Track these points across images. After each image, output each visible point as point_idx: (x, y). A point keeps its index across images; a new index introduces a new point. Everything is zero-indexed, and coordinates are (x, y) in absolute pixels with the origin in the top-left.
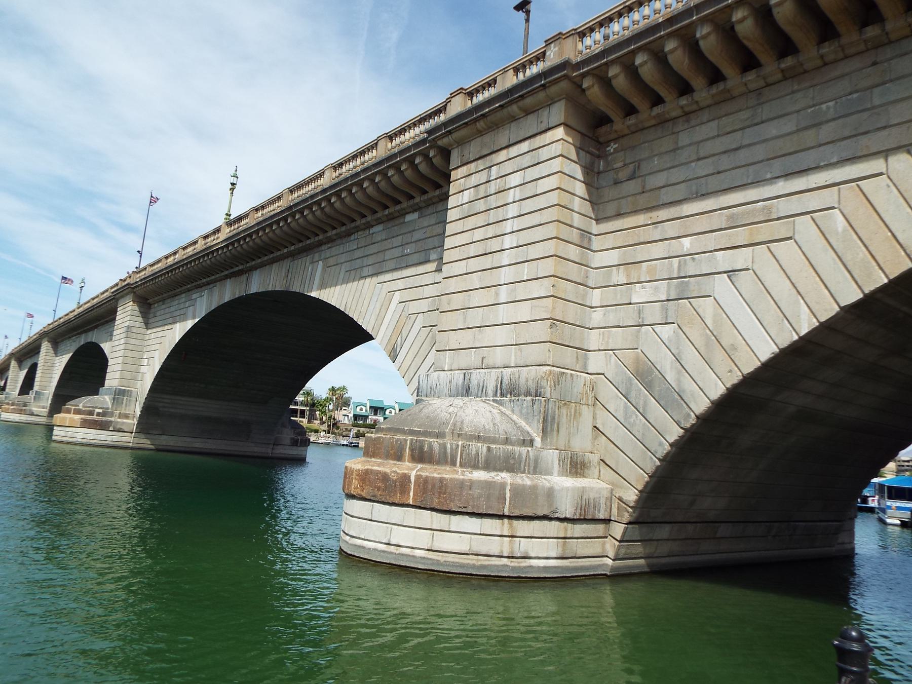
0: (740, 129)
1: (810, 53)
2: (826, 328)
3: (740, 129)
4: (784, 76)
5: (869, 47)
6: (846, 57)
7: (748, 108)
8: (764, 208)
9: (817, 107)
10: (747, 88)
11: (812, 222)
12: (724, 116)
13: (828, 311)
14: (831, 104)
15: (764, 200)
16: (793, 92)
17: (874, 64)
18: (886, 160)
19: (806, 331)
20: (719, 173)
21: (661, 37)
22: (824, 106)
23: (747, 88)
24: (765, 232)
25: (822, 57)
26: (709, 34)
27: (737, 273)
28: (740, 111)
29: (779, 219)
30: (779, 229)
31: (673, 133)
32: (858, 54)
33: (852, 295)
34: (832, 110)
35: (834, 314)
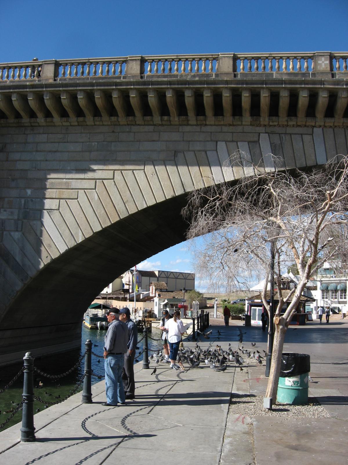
0: (57, 142)
1: (283, 118)
2: (87, 241)
3: (57, 142)
4: (78, 124)
5: (112, 124)
6: (103, 125)
7: (61, 133)
8: (66, 183)
9: (91, 143)
10: (233, 123)
11: (84, 193)
12: (50, 134)
13: (89, 234)
14: (96, 143)
15: (66, 179)
16: (81, 133)
17: (113, 132)
18: (317, 163)
19: (81, 241)
20: (46, 160)
21: (204, 88)
22: (93, 144)
23: (233, 123)
24: (66, 193)
25: (31, 123)
26: (247, 96)
27: (52, 211)
28: (58, 133)
29: (72, 189)
30: (72, 193)
31: (24, 134)
32: (108, 125)
33: (98, 228)
34: (96, 146)
35: (91, 235)
